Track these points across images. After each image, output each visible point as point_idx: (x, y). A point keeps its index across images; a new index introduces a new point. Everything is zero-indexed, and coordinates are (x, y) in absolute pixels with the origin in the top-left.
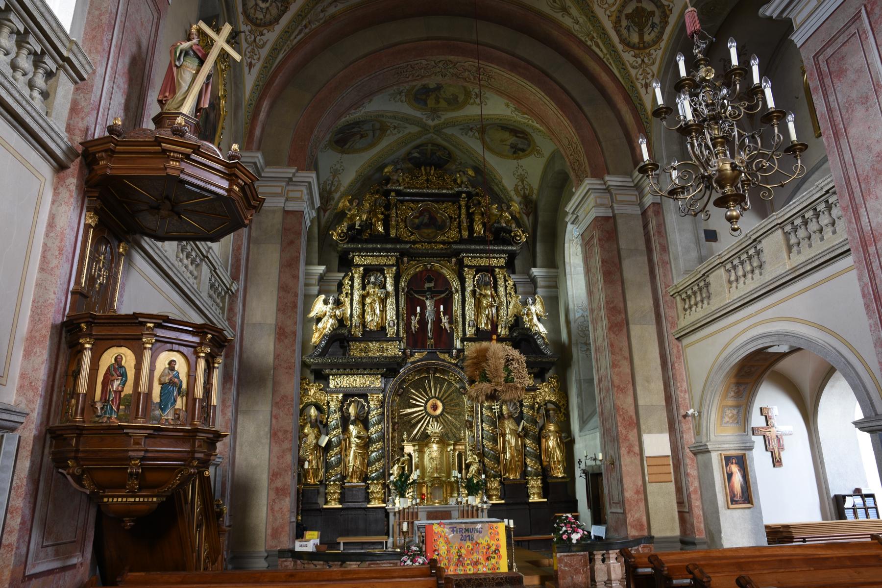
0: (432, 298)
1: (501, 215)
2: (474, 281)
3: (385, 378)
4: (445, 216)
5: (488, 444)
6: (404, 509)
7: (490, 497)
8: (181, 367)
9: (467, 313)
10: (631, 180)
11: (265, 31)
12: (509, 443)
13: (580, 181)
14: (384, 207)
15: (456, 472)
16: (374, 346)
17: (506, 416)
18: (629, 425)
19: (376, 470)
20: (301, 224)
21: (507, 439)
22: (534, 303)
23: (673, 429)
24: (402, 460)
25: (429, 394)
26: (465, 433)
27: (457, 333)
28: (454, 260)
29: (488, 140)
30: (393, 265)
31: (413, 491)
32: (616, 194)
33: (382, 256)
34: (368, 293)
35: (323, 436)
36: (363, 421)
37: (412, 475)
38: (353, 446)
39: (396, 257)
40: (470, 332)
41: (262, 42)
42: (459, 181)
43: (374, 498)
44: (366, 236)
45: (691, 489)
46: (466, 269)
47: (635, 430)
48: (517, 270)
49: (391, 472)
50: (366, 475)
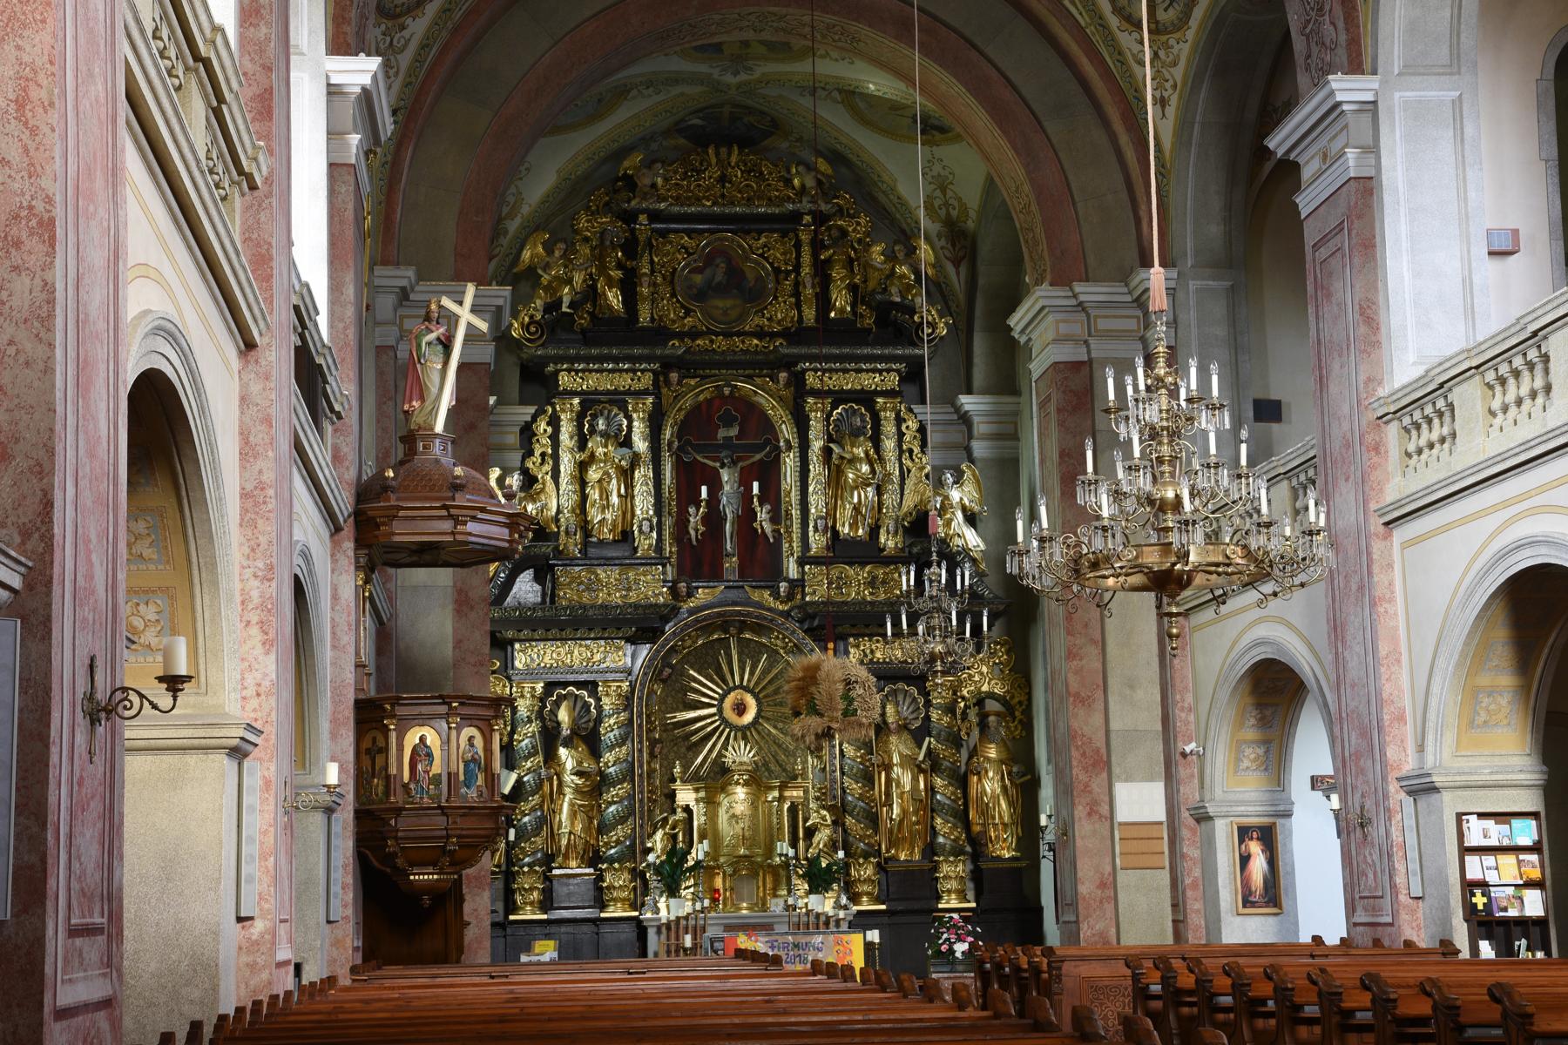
0: (734, 463)
1: (893, 268)
5: (855, 788)
6: (678, 919)
7: (855, 898)
8: (479, 742)
9: (812, 499)
10: (1126, 290)
11: (409, 21)
15: (785, 845)
17: (893, 727)
18: (1094, 765)
19: (618, 842)
22: (958, 481)
23: (1171, 768)
25: (728, 677)
26: (805, 762)
27: (791, 542)
30: (646, 392)
31: (695, 885)
32: (1096, 317)
33: (621, 371)
34: (592, 455)
36: (588, 737)
37: (694, 851)
38: (567, 790)
40: (817, 542)
41: (403, 41)
43: (615, 900)
45: (1188, 881)
47: (1105, 775)
49: (649, 845)
50: (597, 852)
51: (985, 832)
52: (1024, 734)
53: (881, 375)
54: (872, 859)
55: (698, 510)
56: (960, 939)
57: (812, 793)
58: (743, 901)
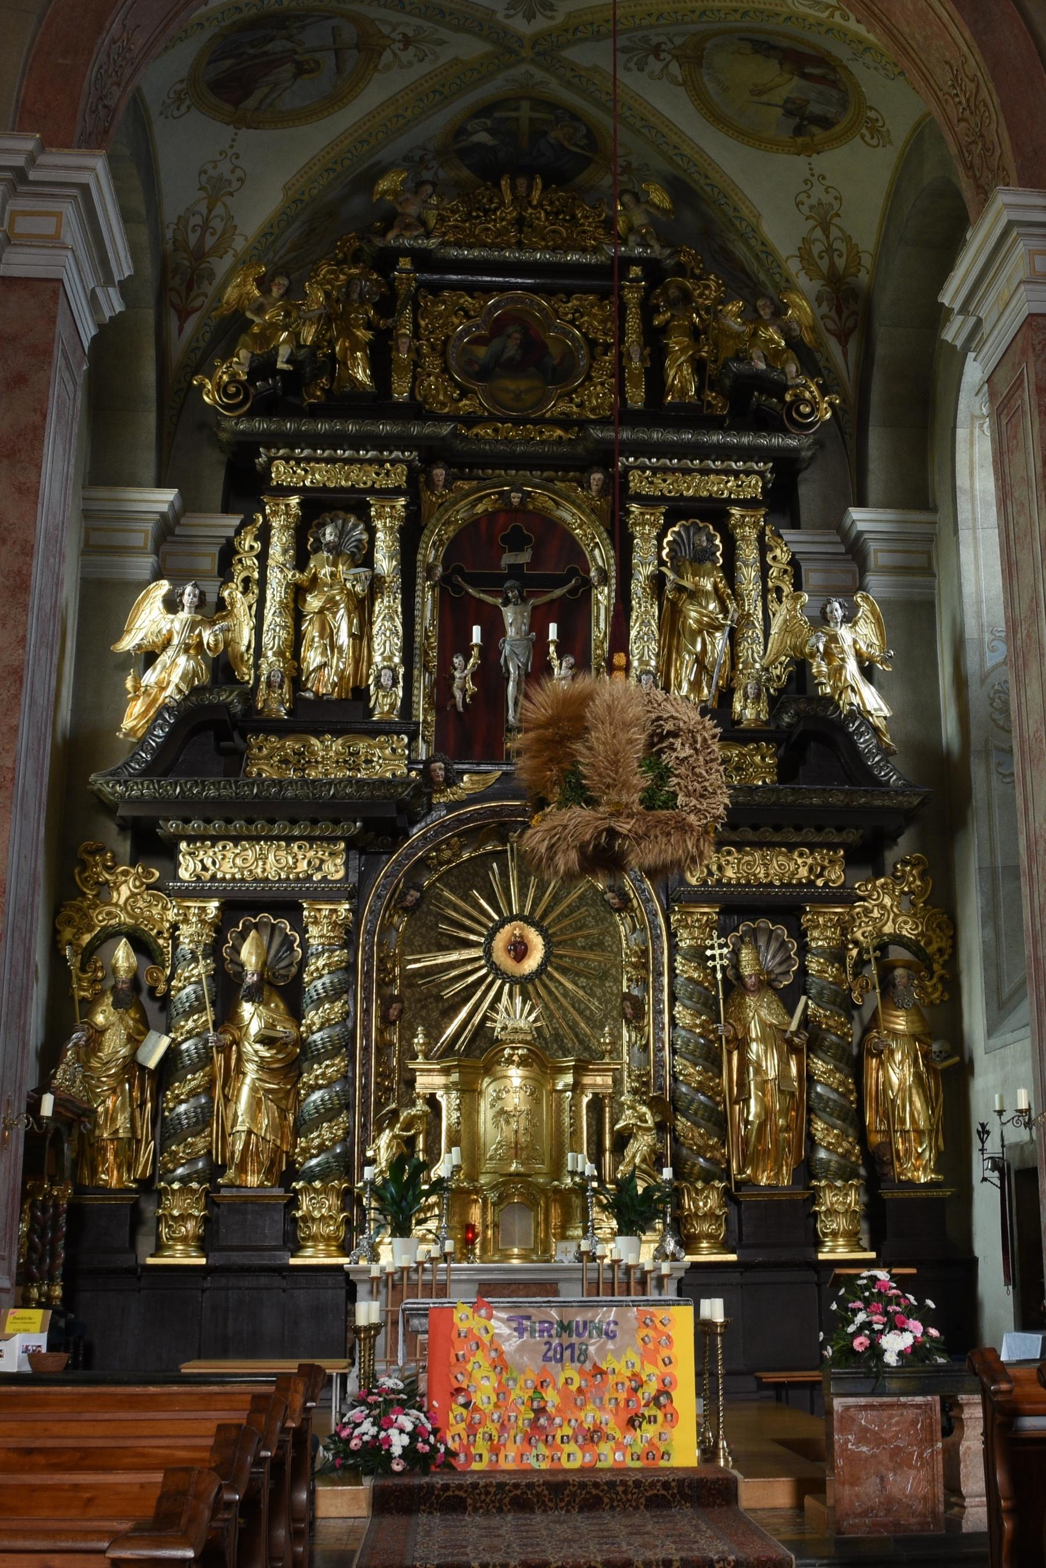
1: (755, 334)
2: (660, 548)
3: (362, 852)
4: (574, 338)
5: (692, 1072)
7: (688, 1243)
12: (758, 1070)
13: (984, 195)
14: (376, 306)
16: (327, 749)
17: (750, 982)
19: (322, 1148)
20: (52, 320)
21: (753, 1056)
22: (850, 618)
24: (404, 1115)
26: (617, 1038)
28: (596, 477)
29: (711, 87)
30: (397, 492)
33: (362, 461)
34: (315, 578)
35: (153, 1035)
38: (251, 1068)
39: (409, 463)
42: (621, 226)
43: (313, 1238)
44: (316, 395)
46: (635, 508)
48: (804, 516)
49: (370, 1154)
50: (291, 1163)
51: (889, 1144)
52: (946, 997)
53: (737, 477)
54: (716, 1183)
55: (467, 661)
56: (894, 1325)
57: (627, 1084)
58: (513, 1244)
